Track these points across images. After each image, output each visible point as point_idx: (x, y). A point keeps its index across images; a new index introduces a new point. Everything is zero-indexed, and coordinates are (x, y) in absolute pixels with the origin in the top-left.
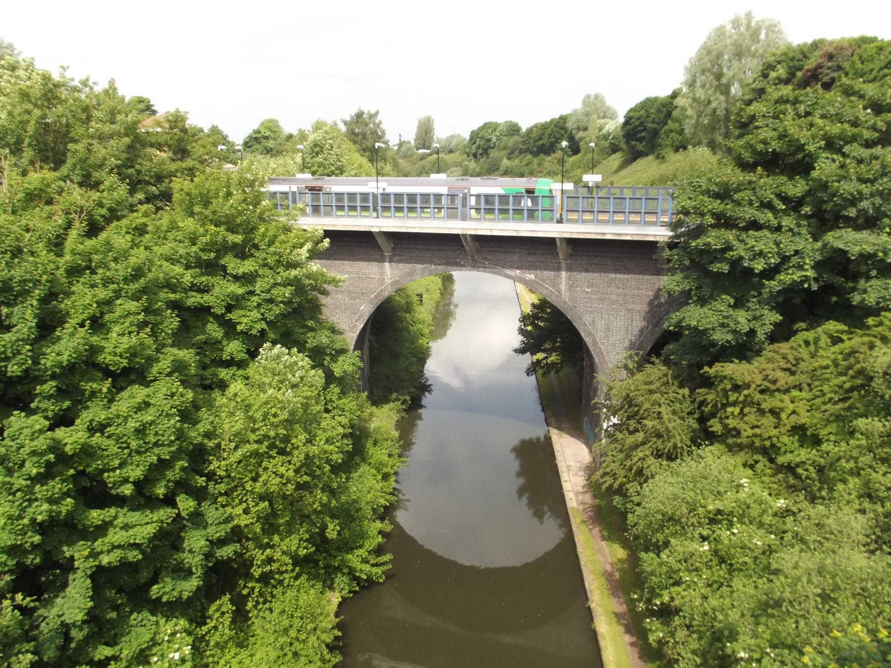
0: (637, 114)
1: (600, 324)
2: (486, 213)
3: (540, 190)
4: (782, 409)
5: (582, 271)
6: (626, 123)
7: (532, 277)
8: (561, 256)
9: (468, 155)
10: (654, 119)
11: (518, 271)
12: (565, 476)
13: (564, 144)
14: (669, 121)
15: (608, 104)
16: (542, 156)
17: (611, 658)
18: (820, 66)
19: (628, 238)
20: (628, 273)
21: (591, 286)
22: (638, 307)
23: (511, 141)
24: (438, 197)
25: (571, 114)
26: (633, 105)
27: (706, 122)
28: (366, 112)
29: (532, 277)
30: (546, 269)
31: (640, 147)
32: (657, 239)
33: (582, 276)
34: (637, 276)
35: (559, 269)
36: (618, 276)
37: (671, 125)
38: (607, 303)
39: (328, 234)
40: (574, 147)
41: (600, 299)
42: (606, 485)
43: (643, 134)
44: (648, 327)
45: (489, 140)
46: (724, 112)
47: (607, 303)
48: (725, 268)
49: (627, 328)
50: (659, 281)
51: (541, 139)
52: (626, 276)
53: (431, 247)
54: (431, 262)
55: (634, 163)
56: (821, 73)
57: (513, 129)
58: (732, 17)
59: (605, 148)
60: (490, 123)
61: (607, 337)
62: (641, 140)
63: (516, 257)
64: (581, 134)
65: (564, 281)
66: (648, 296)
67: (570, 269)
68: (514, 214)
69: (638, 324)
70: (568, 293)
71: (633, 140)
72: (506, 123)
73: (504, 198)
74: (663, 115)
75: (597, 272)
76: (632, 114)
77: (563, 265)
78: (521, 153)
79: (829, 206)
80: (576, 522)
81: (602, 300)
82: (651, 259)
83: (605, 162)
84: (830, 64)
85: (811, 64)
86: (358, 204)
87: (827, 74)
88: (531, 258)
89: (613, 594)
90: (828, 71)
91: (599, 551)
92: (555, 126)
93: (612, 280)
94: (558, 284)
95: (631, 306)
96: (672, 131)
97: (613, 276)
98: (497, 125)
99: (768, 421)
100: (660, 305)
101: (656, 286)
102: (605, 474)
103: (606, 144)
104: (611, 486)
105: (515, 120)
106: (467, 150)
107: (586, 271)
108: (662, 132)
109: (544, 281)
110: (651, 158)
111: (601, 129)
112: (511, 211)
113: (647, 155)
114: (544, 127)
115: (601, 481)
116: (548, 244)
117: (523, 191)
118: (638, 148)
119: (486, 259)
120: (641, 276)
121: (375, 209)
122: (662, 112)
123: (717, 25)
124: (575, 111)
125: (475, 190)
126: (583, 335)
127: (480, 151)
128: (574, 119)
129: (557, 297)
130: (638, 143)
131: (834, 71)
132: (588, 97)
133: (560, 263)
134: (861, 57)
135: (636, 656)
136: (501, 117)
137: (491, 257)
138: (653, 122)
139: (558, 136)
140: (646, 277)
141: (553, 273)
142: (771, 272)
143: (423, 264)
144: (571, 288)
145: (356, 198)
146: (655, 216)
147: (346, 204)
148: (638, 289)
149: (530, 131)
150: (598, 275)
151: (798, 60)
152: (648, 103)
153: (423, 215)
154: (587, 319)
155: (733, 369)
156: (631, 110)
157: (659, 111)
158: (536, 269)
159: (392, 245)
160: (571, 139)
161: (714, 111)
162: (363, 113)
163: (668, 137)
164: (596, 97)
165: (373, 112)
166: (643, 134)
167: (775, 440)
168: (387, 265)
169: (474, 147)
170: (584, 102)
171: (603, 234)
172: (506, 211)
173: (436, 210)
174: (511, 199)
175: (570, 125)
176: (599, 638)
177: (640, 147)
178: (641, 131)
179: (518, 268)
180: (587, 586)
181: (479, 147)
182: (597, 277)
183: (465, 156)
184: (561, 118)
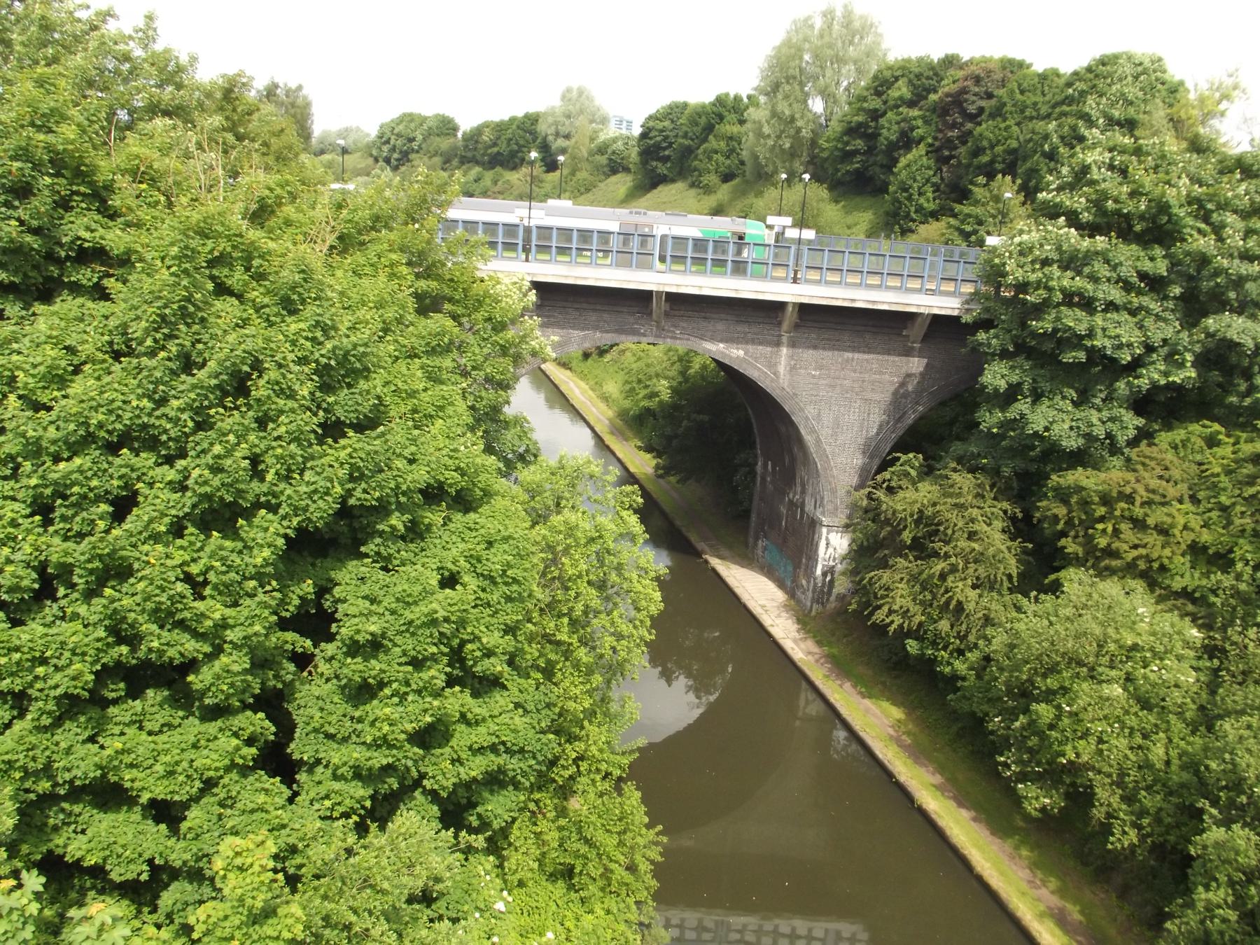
0: (660, 125)
1: (827, 418)
2: (673, 262)
3: (750, 235)
4: (1172, 526)
5: (808, 347)
6: (644, 136)
7: (741, 353)
8: (785, 326)
9: (376, 160)
10: (686, 133)
11: (721, 345)
12: (767, 620)
13: (534, 155)
14: (711, 137)
15: (597, 103)
16: (499, 169)
17: (963, 838)
18: (964, 91)
19: (943, 312)
20: (869, 353)
21: (820, 368)
22: (877, 397)
23: (445, 144)
24: (605, 235)
25: (545, 113)
26: (652, 111)
27: (787, 145)
28: (281, 85)
29: (741, 353)
30: (761, 344)
31: (662, 169)
32: (922, 310)
33: (809, 355)
34: (880, 357)
35: (778, 344)
36: (856, 355)
37: (713, 143)
38: (838, 390)
39: (538, 286)
40: (549, 160)
41: (831, 386)
42: (894, 626)
43: (667, 153)
44: (888, 423)
45: (411, 140)
46: (810, 135)
47: (838, 390)
48: (1082, 356)
49: (862, 424)
50: (908, 362)
51: (495, 144)
52: (866, 356)
53: (598, 307)
54: (596, 328)
55: (655, 191)
56: (966, 101)
57: (446, 126)
58: (824, 8)
59: (602, 166)
60: (410, 115)
61: (834, 435)
62: (665, 159)
63: (720, 326)
64: (561, 142)
65: (783, 360)
66: (892, 383)
67: (793, 344)
68: (713, 265)
69: (876, 418)
70: (788, 377)
71: (653, 159)
72: (437, 116)
73: (700, 244)
74: (699, 129)
75: (829, 349)
76: (651, 124)
77: (784, 339)
78: (462, 163)
79: (1206, 285)
80: (818, 675)
81: (833, 387)
82: (900, 335)
83: (602, 185)
84: (977, 89)
85: (947, 87)
86: (690, 254)
87: (974, 102)
88: (740, 328)
89: (916, 763)
90: (975, 98)
91: (867, 711)
92: (518, 127)
93: (847, 361)
94: (775, 365)
95: (869, 395)
96: (716, 152)
97: (850, 355)
98: (424, 120)
99: (1152, 538)
100: (905, 395)
101: (904, 371)
102: (891, 612)
103: (603, 160)
104: (901, 626)
105: (449, 113)
106: (374, 152)
107: (815, 347)
108: (700, 151)
109: (756, 359)
110: (680, 185)
111: (592, 140)
112: (709, 262)
113: (673, 181)
114: (500, 128)
115: (888, 621)
116: (772, 309)
117: (729, 235)
118: (659, 171)
120: (886, 357)
121: (662, 259)
122: (697, 124)
123: (802, 15)
124: (553, 108)
125: (660, 230)
126: (803, 432)
127: (396, 156)
128: (550, 120)
129: (772, 380)
130: (660, 165)
131: (982, 98)
132: (569, 90)
133: (780, 336)
134: (1020, 85)
135: (988, 833)
136: (429, 107)
138: (685, 136)
139: (522, 142)
140: (892, 358)
141: (769, 349)
142: (1136, 364)
143: (583, 329)
144: (793, 369)
145: (591, 237)
146: (919, 281)
147: (730, 258)
148: (881, 373)
149: (477, 133)
150: (830, 353)
151: (928, 78)
152: (674, 112)
153: (579, 260)
154: (810, 411)
155: (1078, 476)
156: (650, 118)
157: (693, 122)
158: (747, 343)
160: (545, 148)
161: (799, 130)
162: (277, 86)
163: (710, 159)
164: (581, 92)
165: (293, 86)
166: (667, 153)
167: (1166, 561)
168: (784, 350)
169: (385, 148)
170: (563, 98)
171: (853, 300)
172: (702, 261)
173: (600, 254)
174: (711, 244)
175: (542, 128)
176: (934, 816)
177: (662, 169)
178: (665, 149)
179: (721, 341)
180: (881, 756)
181: (393, 149)
182: (827, 356)
183: (370, 161)
184: (527, 116)
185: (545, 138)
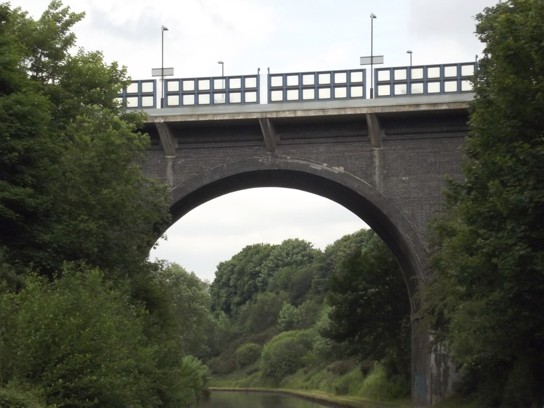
63: (322, 149)
119: (288, 154)
137: (294, 151)
159: (177, 146)
169: (223, 293)
171: (418, 105)
179: (325, 161)
185: (28, 323)
